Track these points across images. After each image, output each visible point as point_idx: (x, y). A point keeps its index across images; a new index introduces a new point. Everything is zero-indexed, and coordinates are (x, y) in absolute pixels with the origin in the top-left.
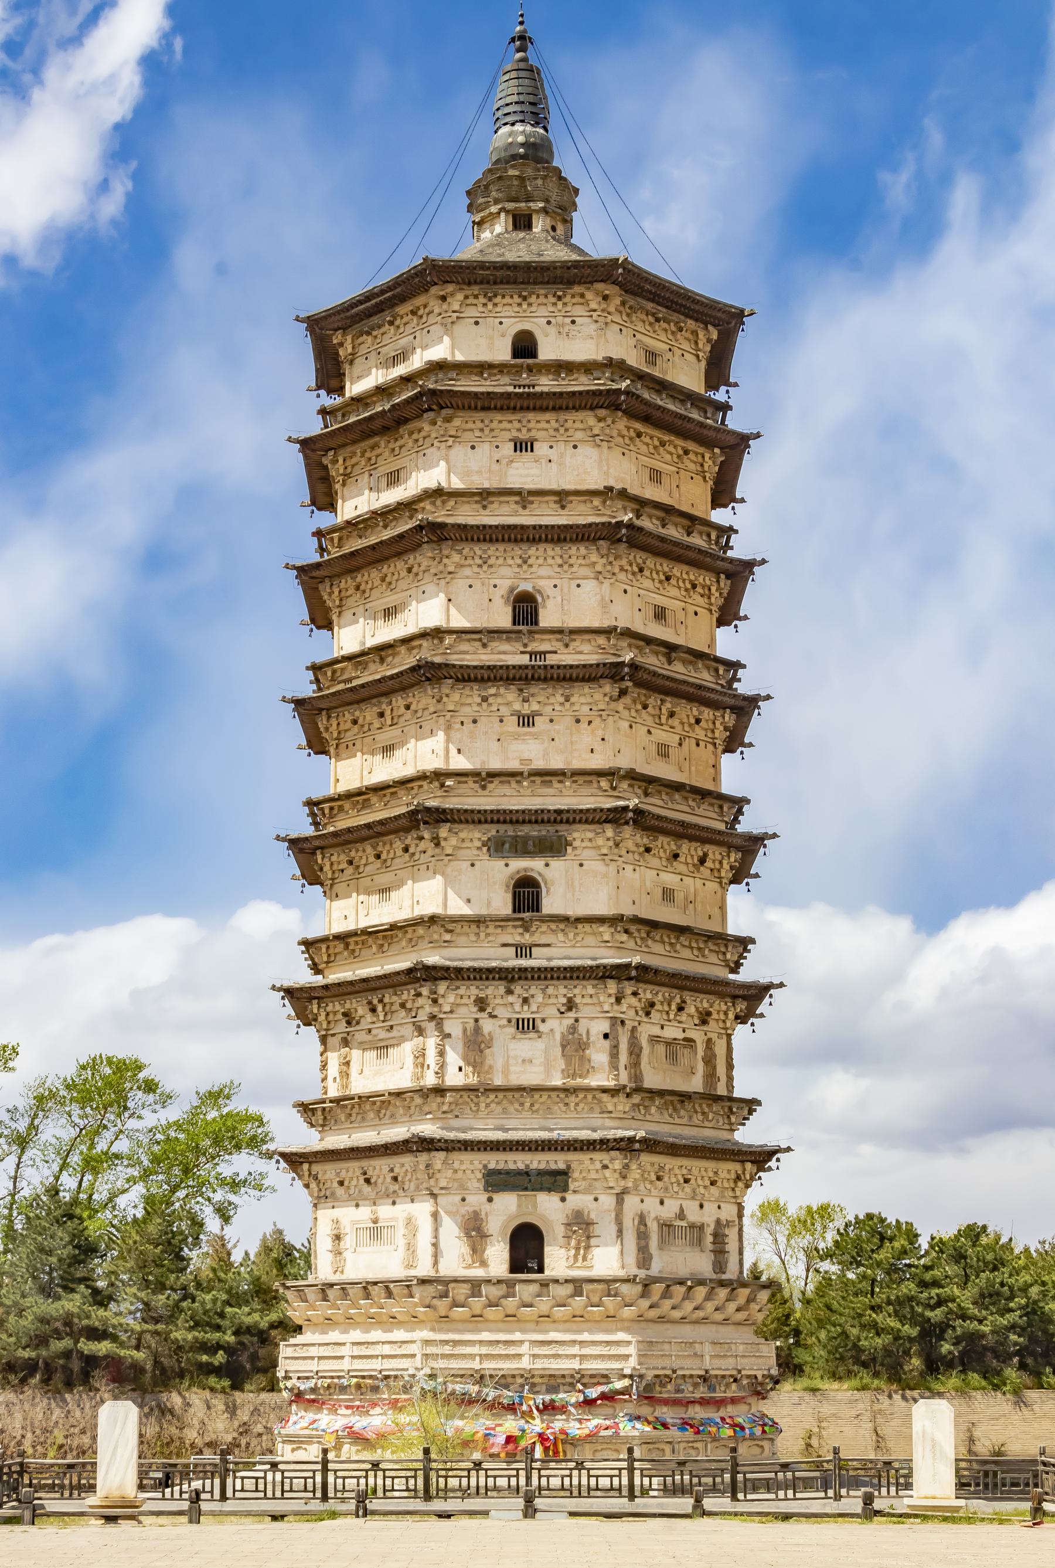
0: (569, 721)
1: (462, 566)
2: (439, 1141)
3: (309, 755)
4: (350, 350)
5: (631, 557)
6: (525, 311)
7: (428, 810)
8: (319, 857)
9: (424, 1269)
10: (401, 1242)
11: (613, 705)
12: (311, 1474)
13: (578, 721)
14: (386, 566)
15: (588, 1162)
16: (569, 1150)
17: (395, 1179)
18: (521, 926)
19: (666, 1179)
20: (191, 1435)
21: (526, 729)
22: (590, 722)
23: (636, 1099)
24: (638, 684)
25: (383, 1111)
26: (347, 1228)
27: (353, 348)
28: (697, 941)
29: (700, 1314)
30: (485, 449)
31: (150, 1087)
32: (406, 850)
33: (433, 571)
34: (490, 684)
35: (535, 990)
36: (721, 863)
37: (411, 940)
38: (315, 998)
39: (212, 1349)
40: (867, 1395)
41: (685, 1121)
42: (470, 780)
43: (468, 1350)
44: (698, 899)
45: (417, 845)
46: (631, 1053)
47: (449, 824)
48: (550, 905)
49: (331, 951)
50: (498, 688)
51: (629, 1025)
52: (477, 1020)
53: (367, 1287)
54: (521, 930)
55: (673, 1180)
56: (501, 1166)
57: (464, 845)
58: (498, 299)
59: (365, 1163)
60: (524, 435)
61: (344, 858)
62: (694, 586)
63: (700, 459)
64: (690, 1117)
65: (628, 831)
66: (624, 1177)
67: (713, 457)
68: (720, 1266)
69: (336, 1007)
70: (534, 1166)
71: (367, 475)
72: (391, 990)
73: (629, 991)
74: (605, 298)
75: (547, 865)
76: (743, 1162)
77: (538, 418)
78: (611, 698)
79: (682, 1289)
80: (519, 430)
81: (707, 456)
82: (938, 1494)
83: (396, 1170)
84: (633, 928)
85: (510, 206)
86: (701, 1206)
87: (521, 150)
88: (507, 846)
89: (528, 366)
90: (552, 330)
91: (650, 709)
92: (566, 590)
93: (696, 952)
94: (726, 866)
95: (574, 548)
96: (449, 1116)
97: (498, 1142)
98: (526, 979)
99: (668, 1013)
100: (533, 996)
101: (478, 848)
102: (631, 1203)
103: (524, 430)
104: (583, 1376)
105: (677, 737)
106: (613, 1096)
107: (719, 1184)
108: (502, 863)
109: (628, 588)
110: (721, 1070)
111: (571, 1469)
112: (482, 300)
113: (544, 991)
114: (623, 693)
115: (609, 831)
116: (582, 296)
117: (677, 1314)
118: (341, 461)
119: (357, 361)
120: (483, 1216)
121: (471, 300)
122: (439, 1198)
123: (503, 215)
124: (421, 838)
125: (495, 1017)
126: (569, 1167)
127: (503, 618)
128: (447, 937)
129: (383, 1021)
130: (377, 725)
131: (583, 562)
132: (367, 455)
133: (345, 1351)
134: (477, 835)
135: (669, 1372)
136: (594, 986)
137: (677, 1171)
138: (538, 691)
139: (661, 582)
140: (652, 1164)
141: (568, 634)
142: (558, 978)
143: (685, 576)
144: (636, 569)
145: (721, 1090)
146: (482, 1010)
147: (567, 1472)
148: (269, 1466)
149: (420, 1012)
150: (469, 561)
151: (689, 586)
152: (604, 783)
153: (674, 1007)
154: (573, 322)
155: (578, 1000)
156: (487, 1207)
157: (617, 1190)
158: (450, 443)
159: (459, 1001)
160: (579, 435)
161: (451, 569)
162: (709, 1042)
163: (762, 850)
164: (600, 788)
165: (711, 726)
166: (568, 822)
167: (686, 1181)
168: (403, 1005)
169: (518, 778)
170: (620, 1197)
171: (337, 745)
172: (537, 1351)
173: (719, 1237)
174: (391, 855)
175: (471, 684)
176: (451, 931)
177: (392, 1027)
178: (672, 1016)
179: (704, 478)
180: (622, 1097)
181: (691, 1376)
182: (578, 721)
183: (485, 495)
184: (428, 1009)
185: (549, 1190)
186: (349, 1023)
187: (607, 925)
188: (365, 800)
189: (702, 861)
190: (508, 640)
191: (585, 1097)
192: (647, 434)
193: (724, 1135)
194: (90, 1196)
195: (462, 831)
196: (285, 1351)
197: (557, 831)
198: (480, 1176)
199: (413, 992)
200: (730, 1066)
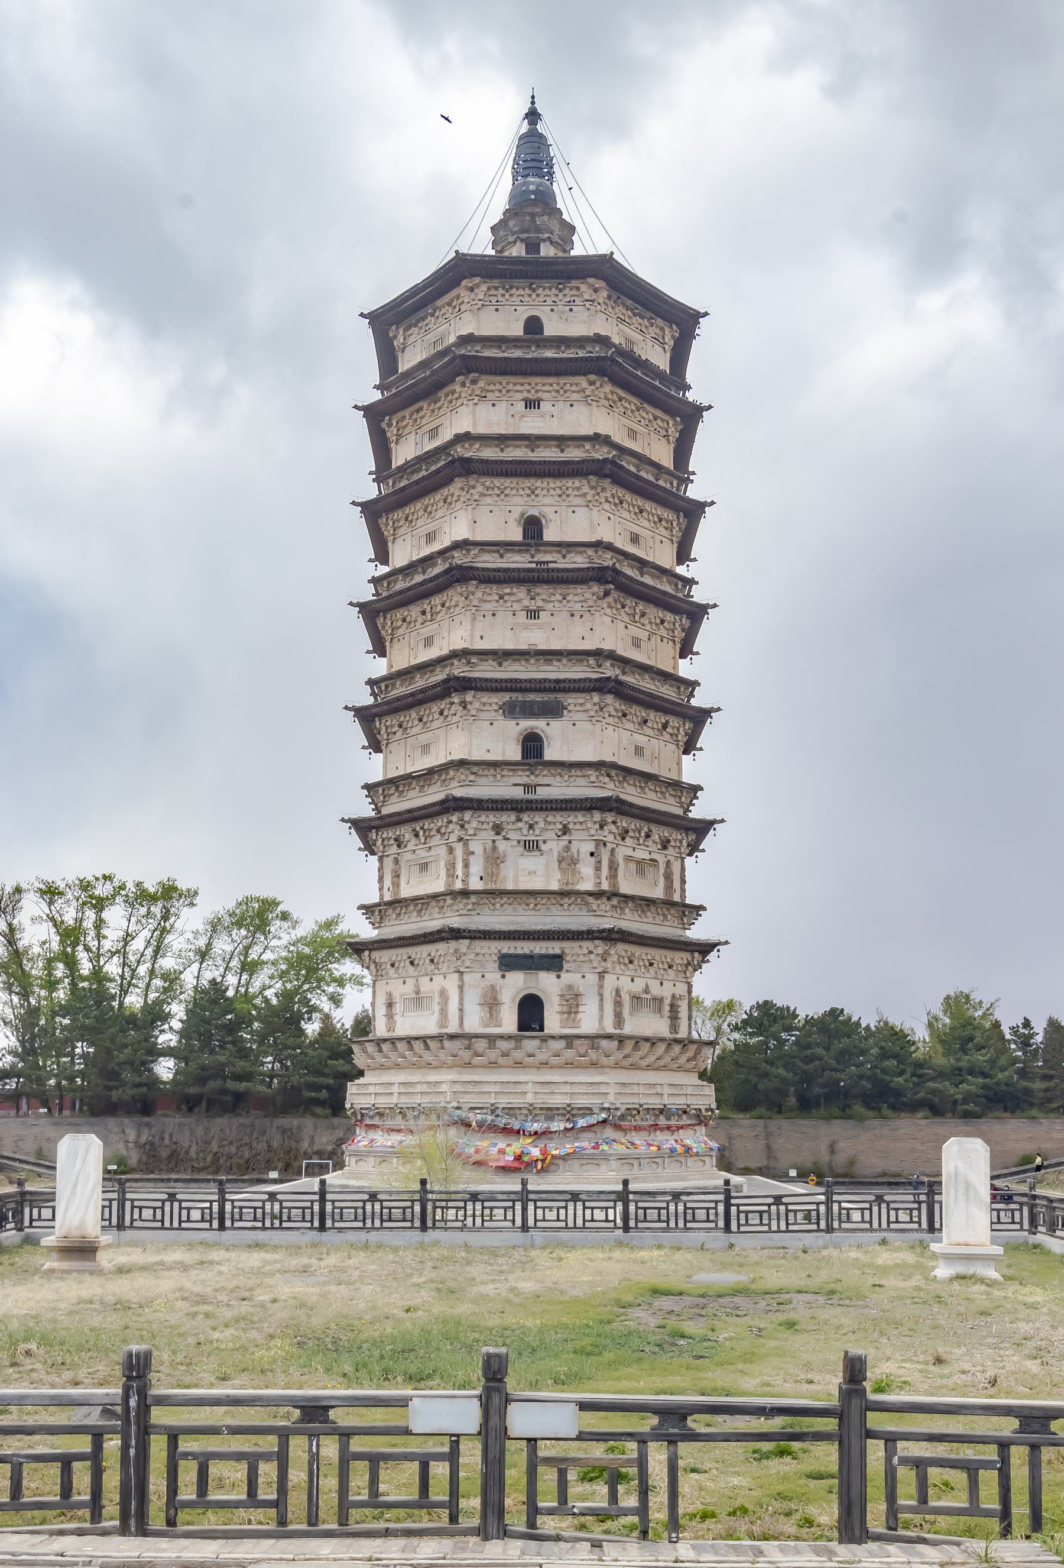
0: (566, 615)
1: (485, 495)
2: (464, 931)
5: (614, 491)
7: (457, 678)
9: (453, 1028)
10: (436, 1008)
11: (599, 602)
12: (308, 1204)
13: (572, 615)
17: (432, 961)
18: (528, 770)
19: (636, 963)
20: (305, 1145)
21: (533, 621)
22: (581, 616)
23: (615, 901)
26: (396, 994)
27: (405, 339)
28: (660, 787)
29: (661, 1063)
30: (502, 406)
31: (285, 916)
33: (462, 499)
35: (539, 818)
36: (678, 729)
37: (444, 780)
38: (374, 828)
39: (318, 1088)
40: (761, 1122)
41: (650, 920)
43: (486, 1088)
44: (661, 756)
45: (449, 709)
46: (610, 868)
48: (549, 754)
51: (610, 846)
52: (494, 841)
53: (409, 1040)
55: (641, 963)
56: (512, 951)
57: (485, 708)
60: (532, 396)
62: (660, 520)
63: (665, 425)
64: (654, 918)
65: (609, 699)
66: (605, 960)
67: (675, 424)
68: (674, 1028)
69: (390, 833)
70: (537, 951)
74: (596, 291)
75: (548, 724)
76: (692, 951)
79: (648, 1045)
80: (529, 391)
81: (671, 423)
82: (971, 1240)
83: (433, 954)
84: (613, 773)
85: (524, 236)
86: (661, 984)
87: (533, 197)
88: (518, 709)
90: (554, 316)
91: (626, 609)
92: (564, 515)
93: (659, 795)
96: (473, 913)
97: (509, 932)
99: (638, 839)
100: (537, 823)
101: (496, 711)
102: (610, 981)
103: (533, 391)
104: (573, 1109)
105: (647, 633)
106: (597, 899)
108: (514, 722)
109: (611, 516)
110: (677, 884)
111: (566, 1201)
112: (501, 291)
114: (607, 594)
115: (596, 698)
116: (578, 289)
117: (644, 1063)
120: (498, 989)
121: (493, 292)
122: (465, 975)
123: (518, 243)
124: (452, 703)
125: (508, 839)
126: (563, 952)
127: (516, 534)
128: (472, 778)
130: (420, 620)
131: (577, 493)
132: (414, 417)
135: (637, 1106)
137: (644, 957)
138: (543, 590)
139: (636, 514)
141: (566, 547)
143: (654, 511)
144: (617, 501)
145: (677, 898)
146: (498, 834)
147: (563, 1204)
148: (266, 1197)
150: (490, 492)
151: (656, 519)
152: (592, 661)
153: (643, 834)
154: (571, 310)
155: (571, 826)
156: (501, 981)
157: (600, 970)
158: (476, 401)
159: (480, 827)
160: (575, 396)
161: (476, 497)
162: (668, 863)
163: (709, 720)
164: (589, 666)
165: (672, 627)
167: (651, 965)
168: (438, 831)
169: (527, 657)
170: (601, 975)
173: (674, 1008)
176: (474, 773)
177: (430, 848)
178: (641, 842)
179: (668, 440)
180: (604, 900)
181: (654, 1109)
182: (572, 615)
184: (457, 832)
185: (548, 969)
186: (399, 846)
189: (665, 726)
190: (519, 551)
192: (626, 400)
193: (679, 932)
194: (247, 989)
196: (352, 1088)
198: (496, 958)
199: (445, 820)
200: (683, 882)
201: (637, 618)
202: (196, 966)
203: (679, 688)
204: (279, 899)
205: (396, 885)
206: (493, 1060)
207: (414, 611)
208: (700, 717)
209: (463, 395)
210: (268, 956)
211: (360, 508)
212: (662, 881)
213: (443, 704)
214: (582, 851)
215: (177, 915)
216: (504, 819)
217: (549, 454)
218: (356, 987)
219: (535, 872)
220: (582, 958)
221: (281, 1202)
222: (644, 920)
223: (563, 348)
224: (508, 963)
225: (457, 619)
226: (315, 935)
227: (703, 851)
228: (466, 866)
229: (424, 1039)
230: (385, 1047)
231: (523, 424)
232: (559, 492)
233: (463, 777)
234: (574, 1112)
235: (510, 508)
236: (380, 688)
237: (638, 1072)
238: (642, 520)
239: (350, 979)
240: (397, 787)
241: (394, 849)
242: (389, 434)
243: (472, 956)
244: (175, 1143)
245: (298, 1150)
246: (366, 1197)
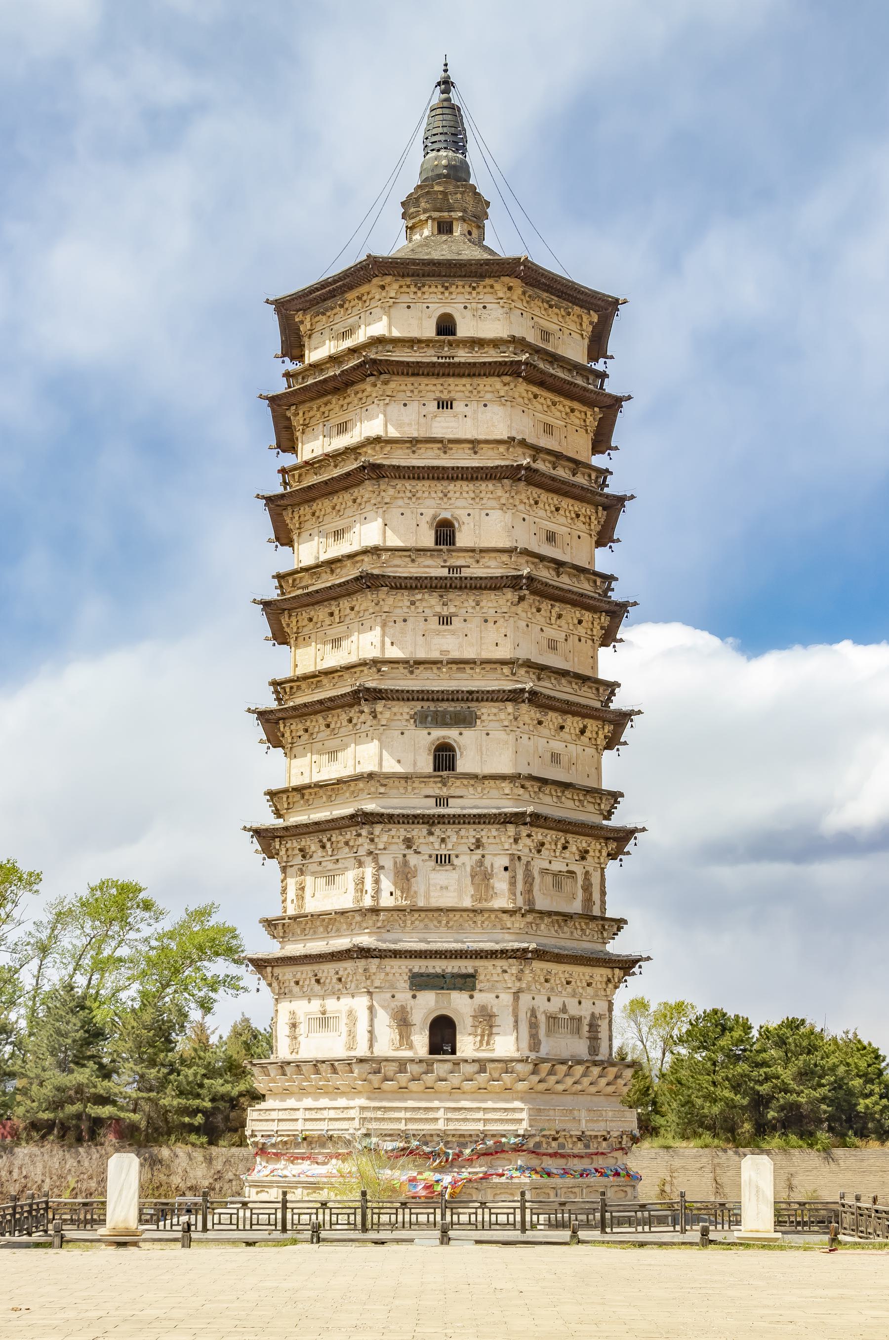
0: (478, 621)
1: (396, 498)
2: (375, 950)
3: (274, 645)
4: (309, 327)
5: (529, 493)
6: (447, 298)
8: (282, 726)
9: (362, 1051)
10: (344, 1029)
11: (514, 608)
13: (486, 621)
14: (335, 498)
15: (491, 968)
16: (476, 958)
17: (340, 980)
20: (176, 1180)
21: (445, 627)
22: (495, 622)
25: (330, 927)
27: (311, 325)
30: (414, 407)
31: (147, 906)
32: (350, 721)
33: (373, 501)
34: (417, 591)
35: (450, 831)
36: (597, 733)
38: (277, 837)
39: (194, 1112)
42: (401, 666)
43: (397, 1115)
45: (359, 718)
52: (405, 856)
53: (316, 1065)
54: (440, 785)
57: (396, 718)
59: (316, 967)
60: (445, 396)
61: (301, 726)
65: (524, 707)
68: (594, 1049)
69: (294, 844)
70: (449, 970)
71: (321, 425)
72: (337, 832)
73: (524, 834)
75: (461, 734)
76: (612, 968)
77: (457, 383)
78: (512, 603)
80: (441, 392)
81: (589, 413)
82: (761, 1228)
84: (528, 784)
85: (436, 215)
88: (429, 719)
89: (449, 341)
90: (468, 313)
92: (477, 518)
93: (577, 803)
94: (601, 736)
95: (484, 485)
98: (444, 823)
99: (555, 851)
100: (449, 837)
101: (407, 720)
102: (525, 999)
103: (445, 392)
107: (594, 985)
108: (425, 732)
111: (476, 1208)
112: (413, 289)
113: (457, 832)
114: (522, 599)
115: (510, 707)
116: (492, 287)
117: (560, 1087)
118: (301, 414)
119: (314, 336)
120: (409, 1010)
123: (430, 222)
125: (419, 853)
126: (476, 971)
127: (428, 539)
128: (382, 790)
131: (491, 496)
132: (322, 409)
134: (406, 710)
136: (497, 830)
140: (542, 970)
145: (596, 911)
146: (409, 847)
147: (473, 1211)
149: (360, 848)
150: (402, 495)
151: (574, 516)
153: (559, 846)
154: (485, 307)
155: (484, 840)
158: (387, 401)
163: (629, 724)
167: (568, 983)
168: (347, 843)
169: (439, 666)
171: (296, 638)
172: (450, 1115)
175: (402, 591)
176: (382, 785)
177: (338, 860)
178: (558, 854)
179: (587, 430)
183: (414, 442)
184: (367, 846)
185: (461, 989)
186: (304, 857)
187: (508, 781)
189: (583, 732)
191: (489, 917)
193: (599, 947)
198: (406, 978)
199: (354, 833)
200: (603, 893)
201: (553, 619)
202: (36, 962)
203: (598, 689)
205: (301, 897)
208: (623, 718)
209: (374, 395)
210: (124, 952)
212: (580, 893)
213: (353, 712)
214: (496, 866)
215: (15, 903)
218: (230, 991)
219: (447, 888)
221: (251, 1209)
224: (420, 982)
225: (367, 624)
227: (628, 853)
228: (377, 881)
229: (332, 1065)
230: (289, 1070)
231: (435, 424)
233: (373, 789)
240: (303, 796)
241: (298, 860)
242: (295, 423)
243: (382, 975)
244: (25, 1177)
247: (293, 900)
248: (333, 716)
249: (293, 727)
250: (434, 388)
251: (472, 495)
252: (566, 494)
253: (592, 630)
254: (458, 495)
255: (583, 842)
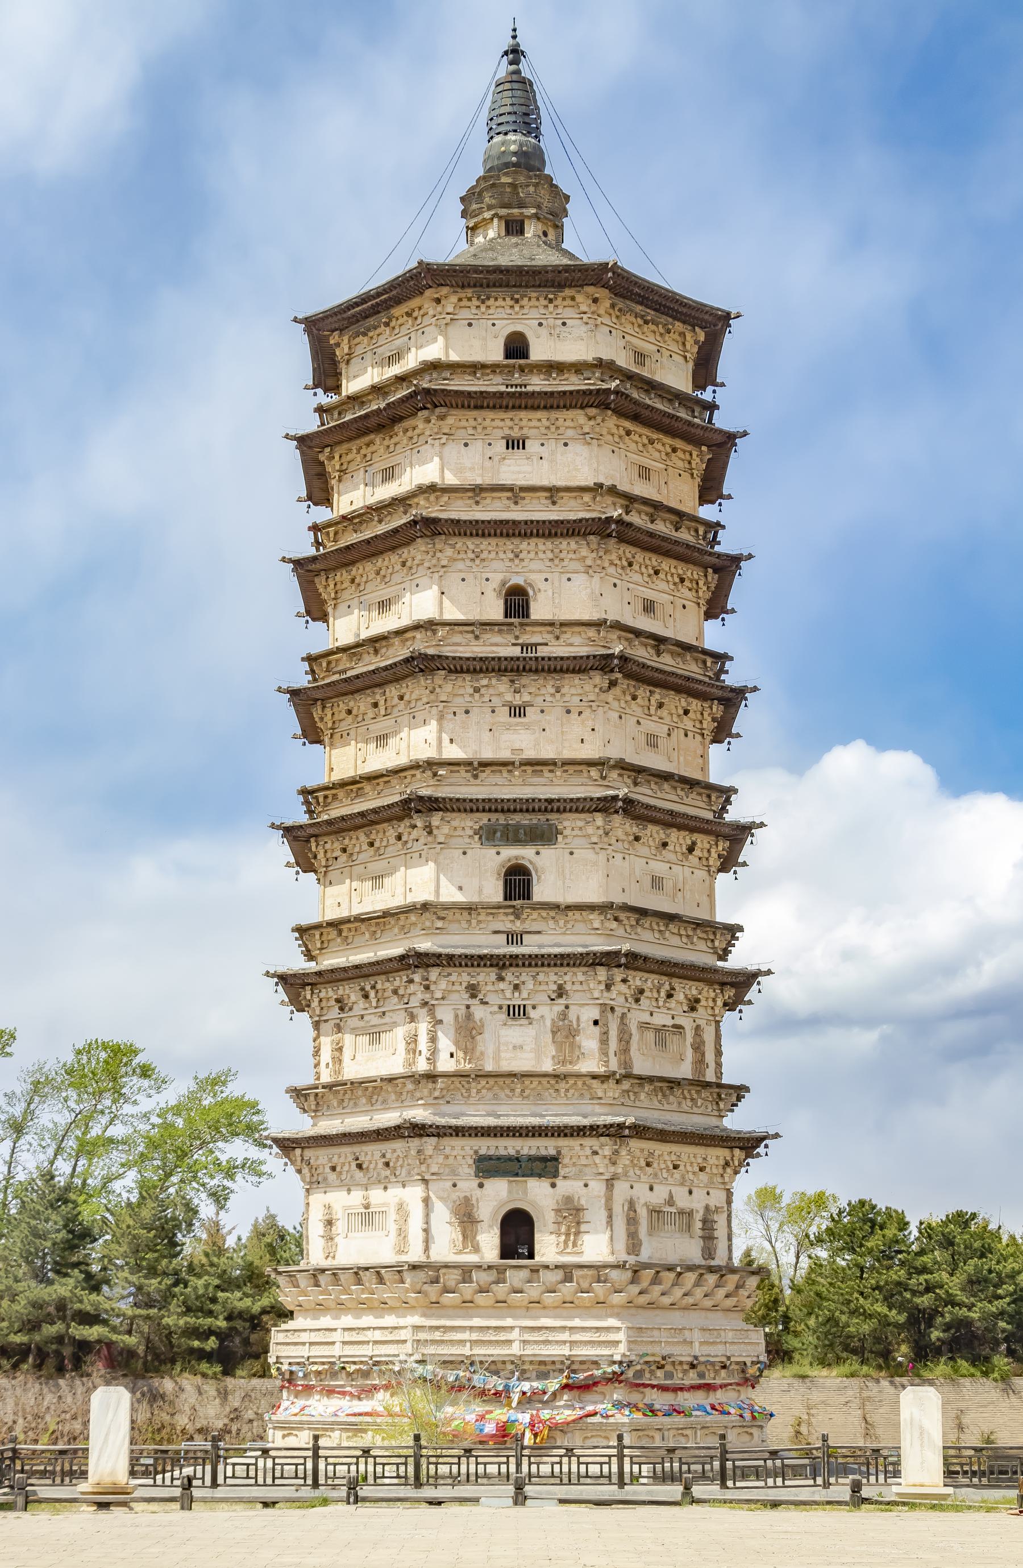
0: (559, 711)
1: (455, 560)
2: (431, 1126)
3: (304, 744)
4: (346, 350)
5: (621, 552)
6: (517, 313)
8: (313, 845)
9: (415, 1254)
10: (393, 1228)
11: (603, 696)
13: (568, 712)
14: (380, 560)
17: (387, 1164)
19: (655, 1165)
20: (182, 1421)
21: (518, 720)
22: (580, 713)
23: (626, 1085)
24: (628, 676)
27: (350, 348)
29: (690, 1300)
31: (145, 1072)
32: (399, 838)
33: (426, 564)
34: (482, 675)
35: (525, 975)
36: (709, 851)
38: (309, 984)
40: (854, 1381)
41: (674, 1107)
44: (687, 887)
45: (410, 834)
47: (441, 813)
49: (324, 938)
50: (490, 679)
51: (619, 1011)
52: (468, 1007)
53: (358, 1272)
54: (512, 918)
55: (663, 1166)
57: (457, 833)
58: (491, 302)
59: (356, 1149)
60: (516, 433)
61: (337, 845)
62: (682, 580)
65: (617, 819)
66: (614, 1164)
67: (701, 454)
68: (708, 1252)
69: (328, 993)
70: (525, 1151)
71: (362, 470)
72: (383, 977)
74: (595, 301)
75: (538, 853)
76: (731, 1148)
77: (530, 417)
78: (601, 689)
79: (672, 1275)
80: (511, 428)
81: (695, 453)
83: (388, 1156)
84: (622, 916)
85: (503, 212)
86: (690, 1192)
87: (514, 159)
88: (498, 834)
89: (520, 366)
90: (543, 331)
92: (556, 584)
93: (685, 940)
95: (565, 543)
98: (517, 965)
99: (657, 1000)
102: (621, 1189)
104: (573, 1362)
107: (708, 1170)
108: (493, 851)
110: (710, 1057)
111: (561, 1456)
112: (475, 302)
113: (534, 977)
114: (613, 684)
115: (599, 819)
116: (573, 299)
117: (666, 1300)
118: (337, 457)
120: (474, 1202)
123: (496, 220)
125: (487, 1003)
126: (559, 1153)
127: (495, 611)
128: (439, 924)
129: (376, 1008)
131: (573, 556)
132: (363, 451)
133: (337, 1336)
134: (469, 823)
137: (667, 1158)
140: (642, 1150)
142: (549, 965)
145: (710, 1076)
146: (473, 996)
147: (557, 1459)
150: (462, 555)
151: (677, 580)
153: (663, 994)
154: (564, 324)
155: (568, 987)
156: (478, 1192)
158: (443, 441)
159: (450, 987)
160: (570, 433)
161: (444, 562)
162: (698, 1027)
163: (749, 839)
166: (558, 811)
167: (676, 1167)
168: (395, 992)
169: (510, 768)
170: (610, 1183)
171: (332, 735)
173: (708, 1224)
174: (384, 844)
175: (464, 675)
177: (384, 1013)
178: (661, 1003)
179: (692, 475)
180: (612, 1082)
182: (568, 712)
183: (477, 491)
185: (540, 1176)
186: (342, 1009)
187: (597, 912)
188: (359, 789)
189: (691, 849)
191: (575, 1084)
193: (713, 1121)
195: (454, 819)
196: (276, 1336)
197: (547, 820)
198: (471, 1162)
199: (405, 979)
200: (719, 1053)
201: (653, 711)
203: (709, 796)
204: (139, 1045)
205: (338, 1060)
206: (468, 1298)
207: (362, 704)
210: (117, 1131)
211: (291, 566)
212: (689, 1053)
213: (403, 827)
216: (481, 978)
217: (539, 511)
220: (584, 1161)
222: (666, 1107)
223: (554, 375)
226: (193, 1098)
228: (433, 1040)
231: (503, 468)
232: (550, 555)
234: (574, 1367)
235: (489, 575)
236: (317, 798)
237: (658, 1312)
238: (658, 582)
239: (243, 1166)
240: (340, 932)
242: (329, 469)
243: (441, 1159)
245: (173, 1426)
246: (359, 1453)
247: (328, 1064)
248: (378, 832)
249: (328, 846)
250: (501, 424)
251: (550, 555)
252: (667, 554)
253: (701, 722)
254: (532, 555)
255: (693, 989)
